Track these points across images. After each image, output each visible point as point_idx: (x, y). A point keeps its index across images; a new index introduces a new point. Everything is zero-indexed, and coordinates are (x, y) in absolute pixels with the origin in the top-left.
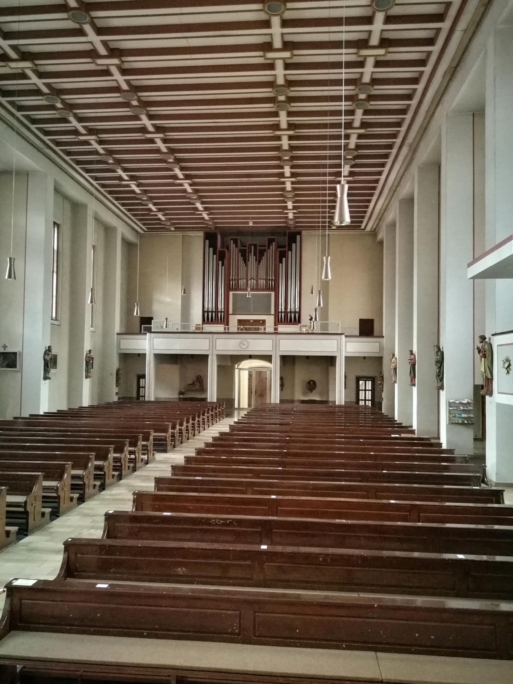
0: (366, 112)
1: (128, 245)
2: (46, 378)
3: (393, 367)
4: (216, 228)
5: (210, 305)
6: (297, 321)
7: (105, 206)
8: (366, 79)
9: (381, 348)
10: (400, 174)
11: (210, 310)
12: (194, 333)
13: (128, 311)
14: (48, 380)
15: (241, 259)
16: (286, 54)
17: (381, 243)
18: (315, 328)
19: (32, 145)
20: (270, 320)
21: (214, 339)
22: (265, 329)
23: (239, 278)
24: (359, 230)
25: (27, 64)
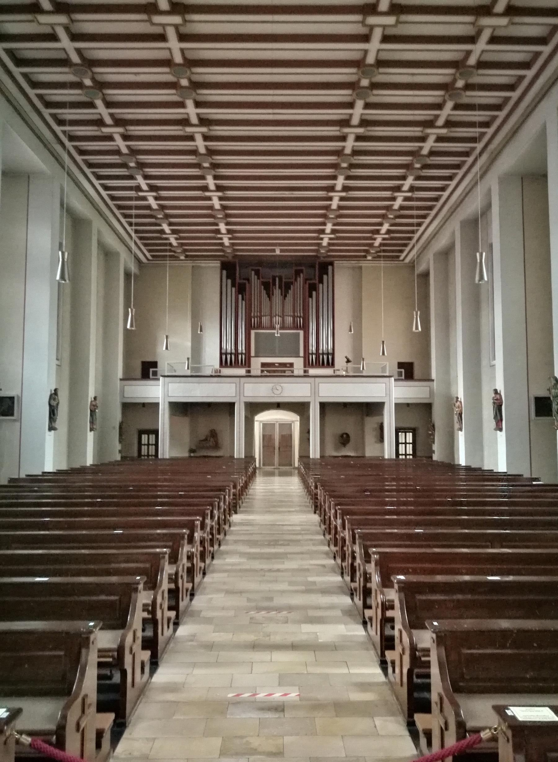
0: (348, 178)
1: (128, 275)
2: (51, 428)
3: (458, 412)
4: (235, 256)
5: (229, 347)
6: (331, 364)
7: (110, 226)
8: (348, 151)
9: (431, 393)
10: (467, 190)
11: (229, 351)
12: (211, 376)
13: (128, 355)
14: (53, 431)
15: (264, 292)
16: (204, 129)
17: (425, 275)
18: (365, 368)
19: (40, 138)
20: (298, 363)
21: (242, 383)
22: (293, 372)
23: (262, 314)
24: (397, 261)
25: (62, 19)
